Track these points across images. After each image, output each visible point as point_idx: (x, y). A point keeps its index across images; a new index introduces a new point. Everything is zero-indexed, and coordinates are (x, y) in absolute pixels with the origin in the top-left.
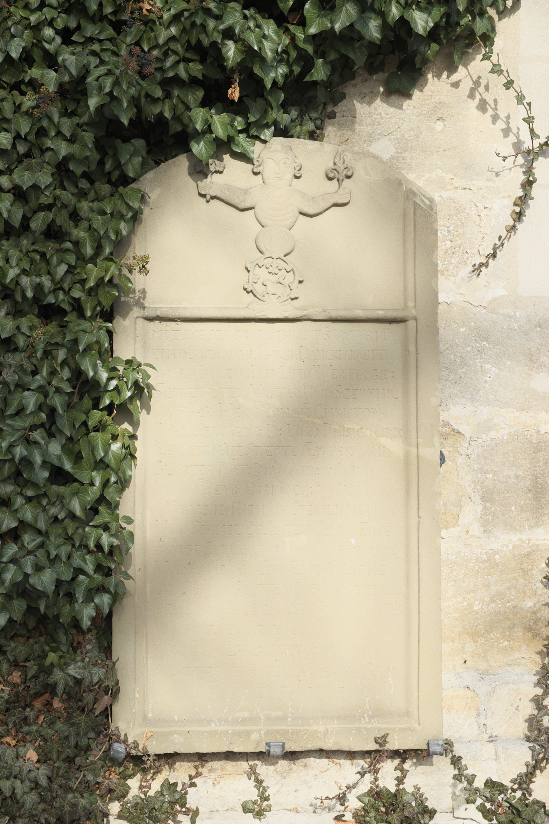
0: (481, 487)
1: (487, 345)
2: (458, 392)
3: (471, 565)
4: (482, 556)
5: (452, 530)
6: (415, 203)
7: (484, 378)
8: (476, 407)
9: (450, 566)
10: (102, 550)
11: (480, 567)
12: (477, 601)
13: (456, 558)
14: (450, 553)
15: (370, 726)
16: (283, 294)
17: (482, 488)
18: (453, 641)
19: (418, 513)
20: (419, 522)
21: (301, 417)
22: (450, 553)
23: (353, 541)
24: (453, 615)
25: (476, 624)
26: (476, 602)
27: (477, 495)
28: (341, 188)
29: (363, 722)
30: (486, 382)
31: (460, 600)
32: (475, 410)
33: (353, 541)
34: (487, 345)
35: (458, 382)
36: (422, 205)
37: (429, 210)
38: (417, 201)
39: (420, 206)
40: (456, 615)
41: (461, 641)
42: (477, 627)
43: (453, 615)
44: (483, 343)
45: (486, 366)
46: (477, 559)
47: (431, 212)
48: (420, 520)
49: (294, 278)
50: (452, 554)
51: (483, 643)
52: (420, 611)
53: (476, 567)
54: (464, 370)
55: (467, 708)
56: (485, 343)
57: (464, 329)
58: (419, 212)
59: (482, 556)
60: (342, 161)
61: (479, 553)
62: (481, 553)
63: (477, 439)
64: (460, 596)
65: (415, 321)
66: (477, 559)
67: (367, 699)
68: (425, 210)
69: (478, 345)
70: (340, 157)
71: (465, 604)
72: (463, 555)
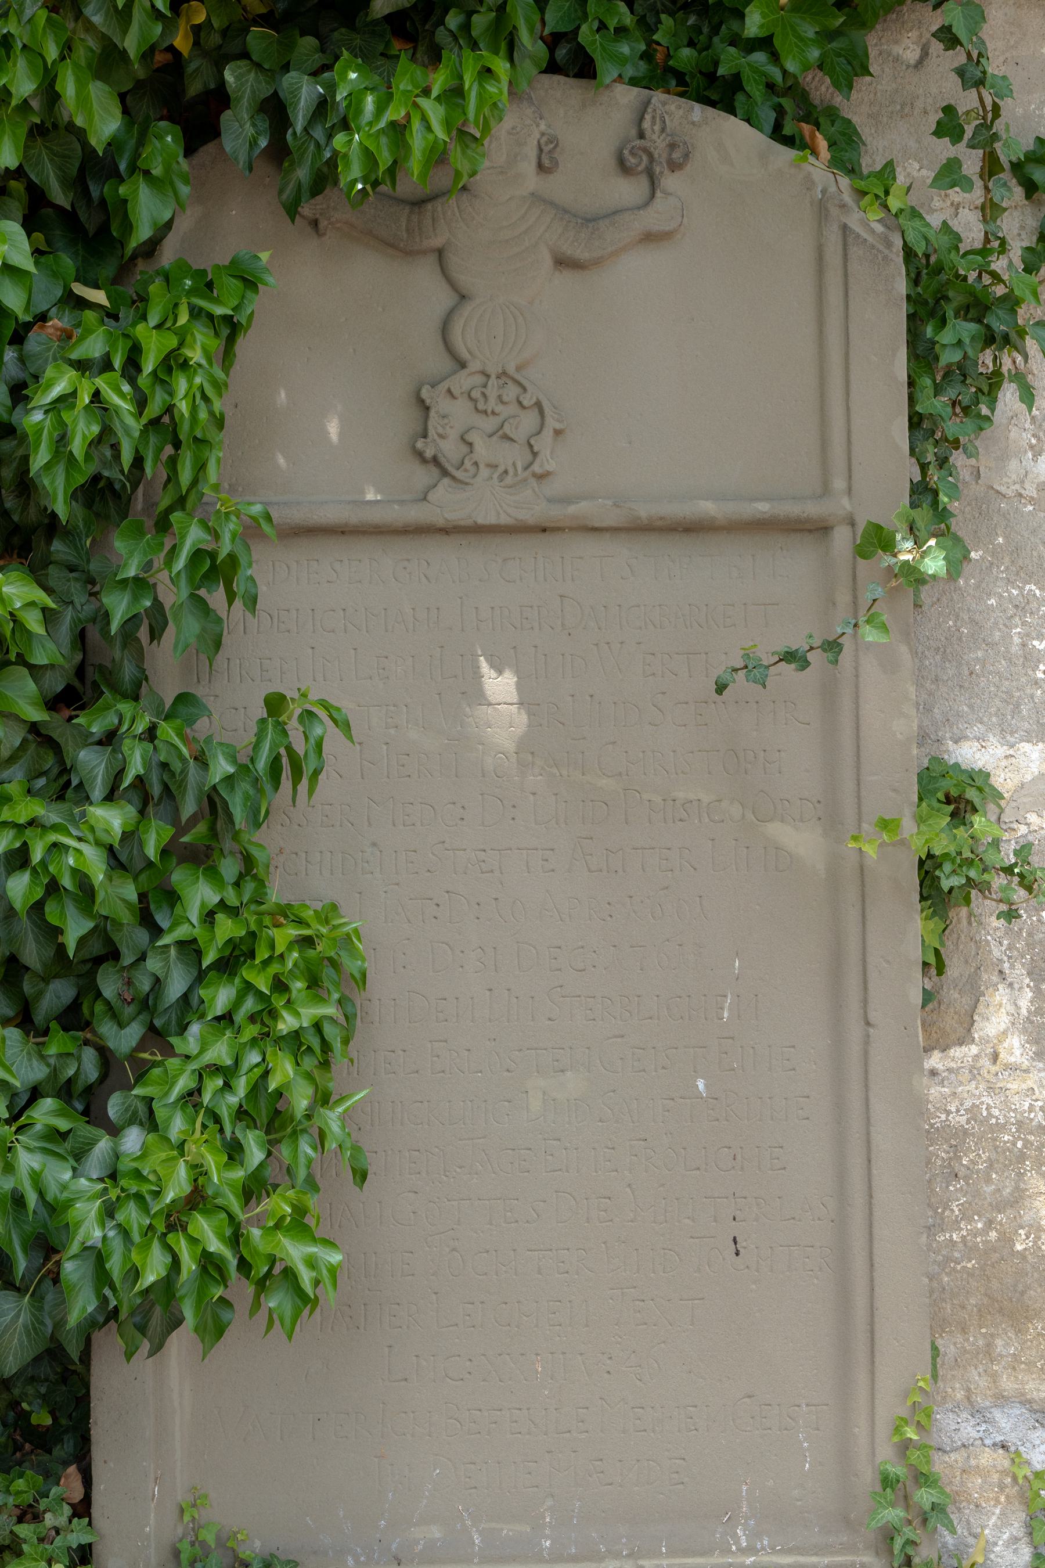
0: (1027, 944)
1: (1038, 592)
2: (966, 709)
3: (1006, 1138)
4: (1032, 1115)
5: (956, 1052)
6: (845, 228)
7: (1030, 672)
8: (1012, 746)
9: (953, 1142)
10: (957, 808)
11: (1027, 1143)
12: (1022, 1228)
13: (968, 1122)
14: (953, 1109)
15: (752, 1559)
16: (514, 464)
17: (1030, 946)
18: (964, 1330)
19: (866, 1013)
20: (868, 1036)
21: (565, 773)
22: (953, 1109)
23: (701, 1084)
24: (964, 1264)
25: (1020, 1287)
26: (1021, 1231)
27: (1018, 965)
28: (658, 194)
29: (734, 1548)
30: (1036, 683)
31: (980, 1225)
32: (1011, 752)
33: (701, 1084)
34: (1038, 592)
35: (966, 685)
36: (864, 235)
37: (881, 247)
38: (850, 225)
39: (858, 236)
40: (969, 1265)
41: (984, 1330)
42: (1023, 1293)
43: (964, 1264)
44: (1027, 587)
45: (1036, 643)
46: (1020, 1124)
47: (886, 251)
48: (871, 1030)
49: (542, 425)
50: (958, 1111)
51: (1039, 1334)
52: (877, 1260)
53: (1020, 1144)
54: (980, 654)
55: (1003, 1499)
56: (1033, 587)
57: (981, 553)
58: (855, 251)
59: (1032, 1115)
60: (657, 128)
61: (1026, 1108)
62: (1031, 1108)
63: (1015, 826)
64: (980, 1216)
65: (849, 528)
66: (1020, 1124)
67: (745, 1488)
68: (873, 247)
69: (1015, 592)
70: (654, 118)
71: (993, 1235)
72: (985, 1114)
